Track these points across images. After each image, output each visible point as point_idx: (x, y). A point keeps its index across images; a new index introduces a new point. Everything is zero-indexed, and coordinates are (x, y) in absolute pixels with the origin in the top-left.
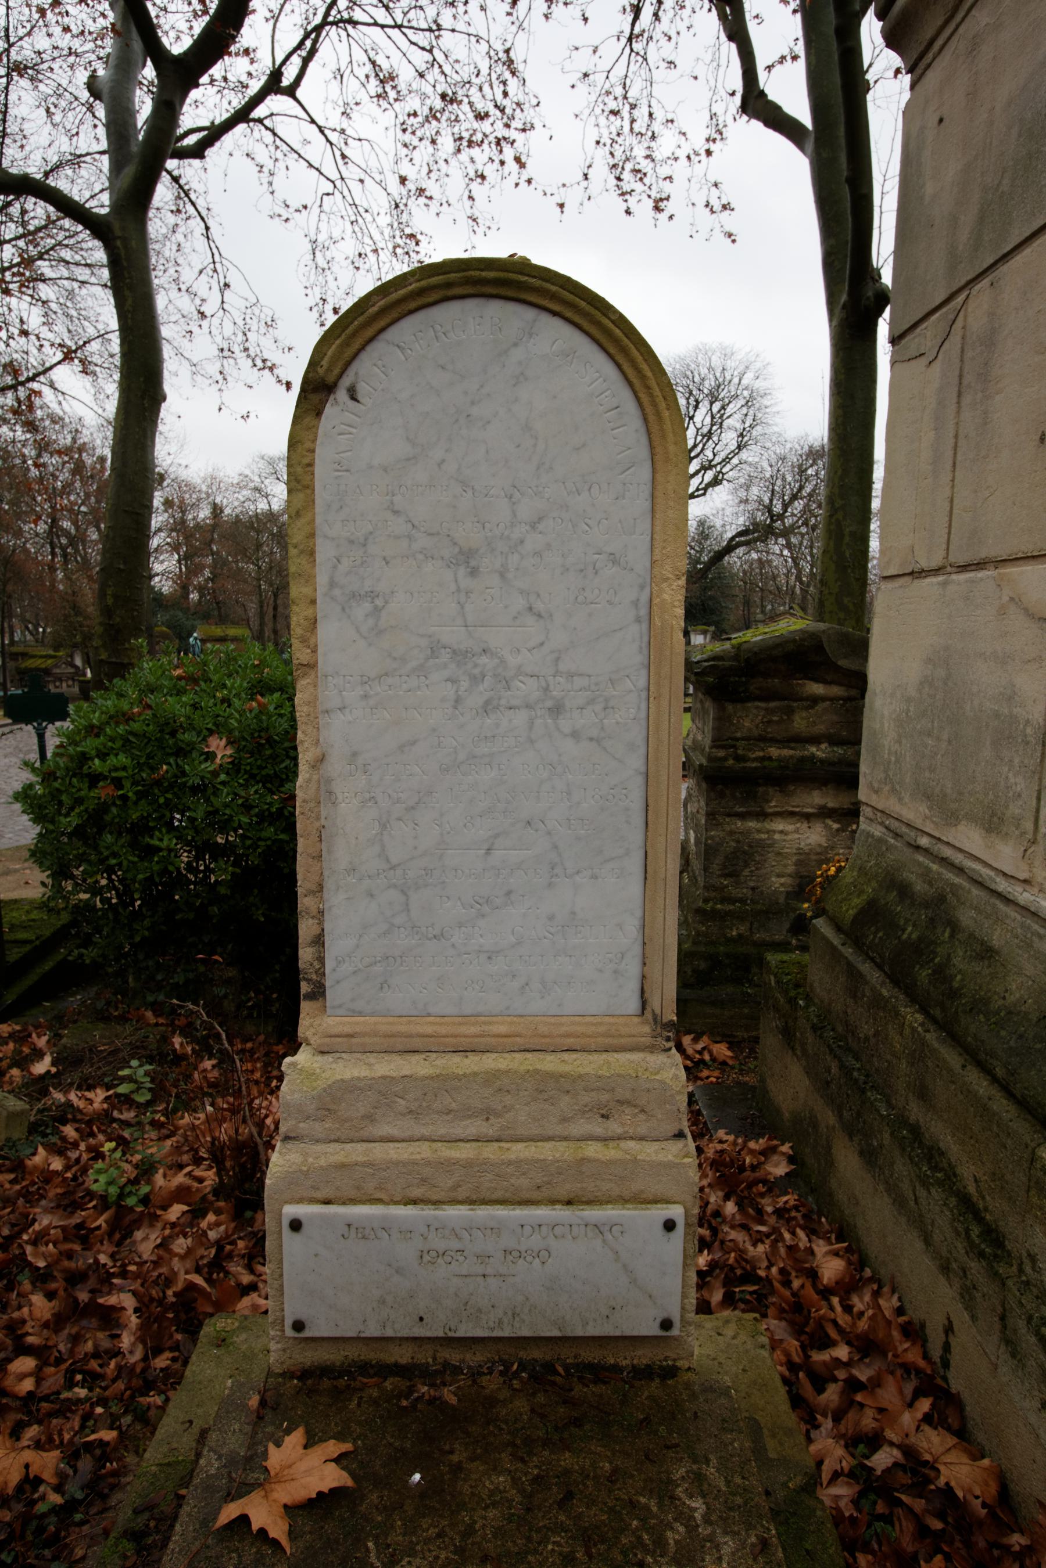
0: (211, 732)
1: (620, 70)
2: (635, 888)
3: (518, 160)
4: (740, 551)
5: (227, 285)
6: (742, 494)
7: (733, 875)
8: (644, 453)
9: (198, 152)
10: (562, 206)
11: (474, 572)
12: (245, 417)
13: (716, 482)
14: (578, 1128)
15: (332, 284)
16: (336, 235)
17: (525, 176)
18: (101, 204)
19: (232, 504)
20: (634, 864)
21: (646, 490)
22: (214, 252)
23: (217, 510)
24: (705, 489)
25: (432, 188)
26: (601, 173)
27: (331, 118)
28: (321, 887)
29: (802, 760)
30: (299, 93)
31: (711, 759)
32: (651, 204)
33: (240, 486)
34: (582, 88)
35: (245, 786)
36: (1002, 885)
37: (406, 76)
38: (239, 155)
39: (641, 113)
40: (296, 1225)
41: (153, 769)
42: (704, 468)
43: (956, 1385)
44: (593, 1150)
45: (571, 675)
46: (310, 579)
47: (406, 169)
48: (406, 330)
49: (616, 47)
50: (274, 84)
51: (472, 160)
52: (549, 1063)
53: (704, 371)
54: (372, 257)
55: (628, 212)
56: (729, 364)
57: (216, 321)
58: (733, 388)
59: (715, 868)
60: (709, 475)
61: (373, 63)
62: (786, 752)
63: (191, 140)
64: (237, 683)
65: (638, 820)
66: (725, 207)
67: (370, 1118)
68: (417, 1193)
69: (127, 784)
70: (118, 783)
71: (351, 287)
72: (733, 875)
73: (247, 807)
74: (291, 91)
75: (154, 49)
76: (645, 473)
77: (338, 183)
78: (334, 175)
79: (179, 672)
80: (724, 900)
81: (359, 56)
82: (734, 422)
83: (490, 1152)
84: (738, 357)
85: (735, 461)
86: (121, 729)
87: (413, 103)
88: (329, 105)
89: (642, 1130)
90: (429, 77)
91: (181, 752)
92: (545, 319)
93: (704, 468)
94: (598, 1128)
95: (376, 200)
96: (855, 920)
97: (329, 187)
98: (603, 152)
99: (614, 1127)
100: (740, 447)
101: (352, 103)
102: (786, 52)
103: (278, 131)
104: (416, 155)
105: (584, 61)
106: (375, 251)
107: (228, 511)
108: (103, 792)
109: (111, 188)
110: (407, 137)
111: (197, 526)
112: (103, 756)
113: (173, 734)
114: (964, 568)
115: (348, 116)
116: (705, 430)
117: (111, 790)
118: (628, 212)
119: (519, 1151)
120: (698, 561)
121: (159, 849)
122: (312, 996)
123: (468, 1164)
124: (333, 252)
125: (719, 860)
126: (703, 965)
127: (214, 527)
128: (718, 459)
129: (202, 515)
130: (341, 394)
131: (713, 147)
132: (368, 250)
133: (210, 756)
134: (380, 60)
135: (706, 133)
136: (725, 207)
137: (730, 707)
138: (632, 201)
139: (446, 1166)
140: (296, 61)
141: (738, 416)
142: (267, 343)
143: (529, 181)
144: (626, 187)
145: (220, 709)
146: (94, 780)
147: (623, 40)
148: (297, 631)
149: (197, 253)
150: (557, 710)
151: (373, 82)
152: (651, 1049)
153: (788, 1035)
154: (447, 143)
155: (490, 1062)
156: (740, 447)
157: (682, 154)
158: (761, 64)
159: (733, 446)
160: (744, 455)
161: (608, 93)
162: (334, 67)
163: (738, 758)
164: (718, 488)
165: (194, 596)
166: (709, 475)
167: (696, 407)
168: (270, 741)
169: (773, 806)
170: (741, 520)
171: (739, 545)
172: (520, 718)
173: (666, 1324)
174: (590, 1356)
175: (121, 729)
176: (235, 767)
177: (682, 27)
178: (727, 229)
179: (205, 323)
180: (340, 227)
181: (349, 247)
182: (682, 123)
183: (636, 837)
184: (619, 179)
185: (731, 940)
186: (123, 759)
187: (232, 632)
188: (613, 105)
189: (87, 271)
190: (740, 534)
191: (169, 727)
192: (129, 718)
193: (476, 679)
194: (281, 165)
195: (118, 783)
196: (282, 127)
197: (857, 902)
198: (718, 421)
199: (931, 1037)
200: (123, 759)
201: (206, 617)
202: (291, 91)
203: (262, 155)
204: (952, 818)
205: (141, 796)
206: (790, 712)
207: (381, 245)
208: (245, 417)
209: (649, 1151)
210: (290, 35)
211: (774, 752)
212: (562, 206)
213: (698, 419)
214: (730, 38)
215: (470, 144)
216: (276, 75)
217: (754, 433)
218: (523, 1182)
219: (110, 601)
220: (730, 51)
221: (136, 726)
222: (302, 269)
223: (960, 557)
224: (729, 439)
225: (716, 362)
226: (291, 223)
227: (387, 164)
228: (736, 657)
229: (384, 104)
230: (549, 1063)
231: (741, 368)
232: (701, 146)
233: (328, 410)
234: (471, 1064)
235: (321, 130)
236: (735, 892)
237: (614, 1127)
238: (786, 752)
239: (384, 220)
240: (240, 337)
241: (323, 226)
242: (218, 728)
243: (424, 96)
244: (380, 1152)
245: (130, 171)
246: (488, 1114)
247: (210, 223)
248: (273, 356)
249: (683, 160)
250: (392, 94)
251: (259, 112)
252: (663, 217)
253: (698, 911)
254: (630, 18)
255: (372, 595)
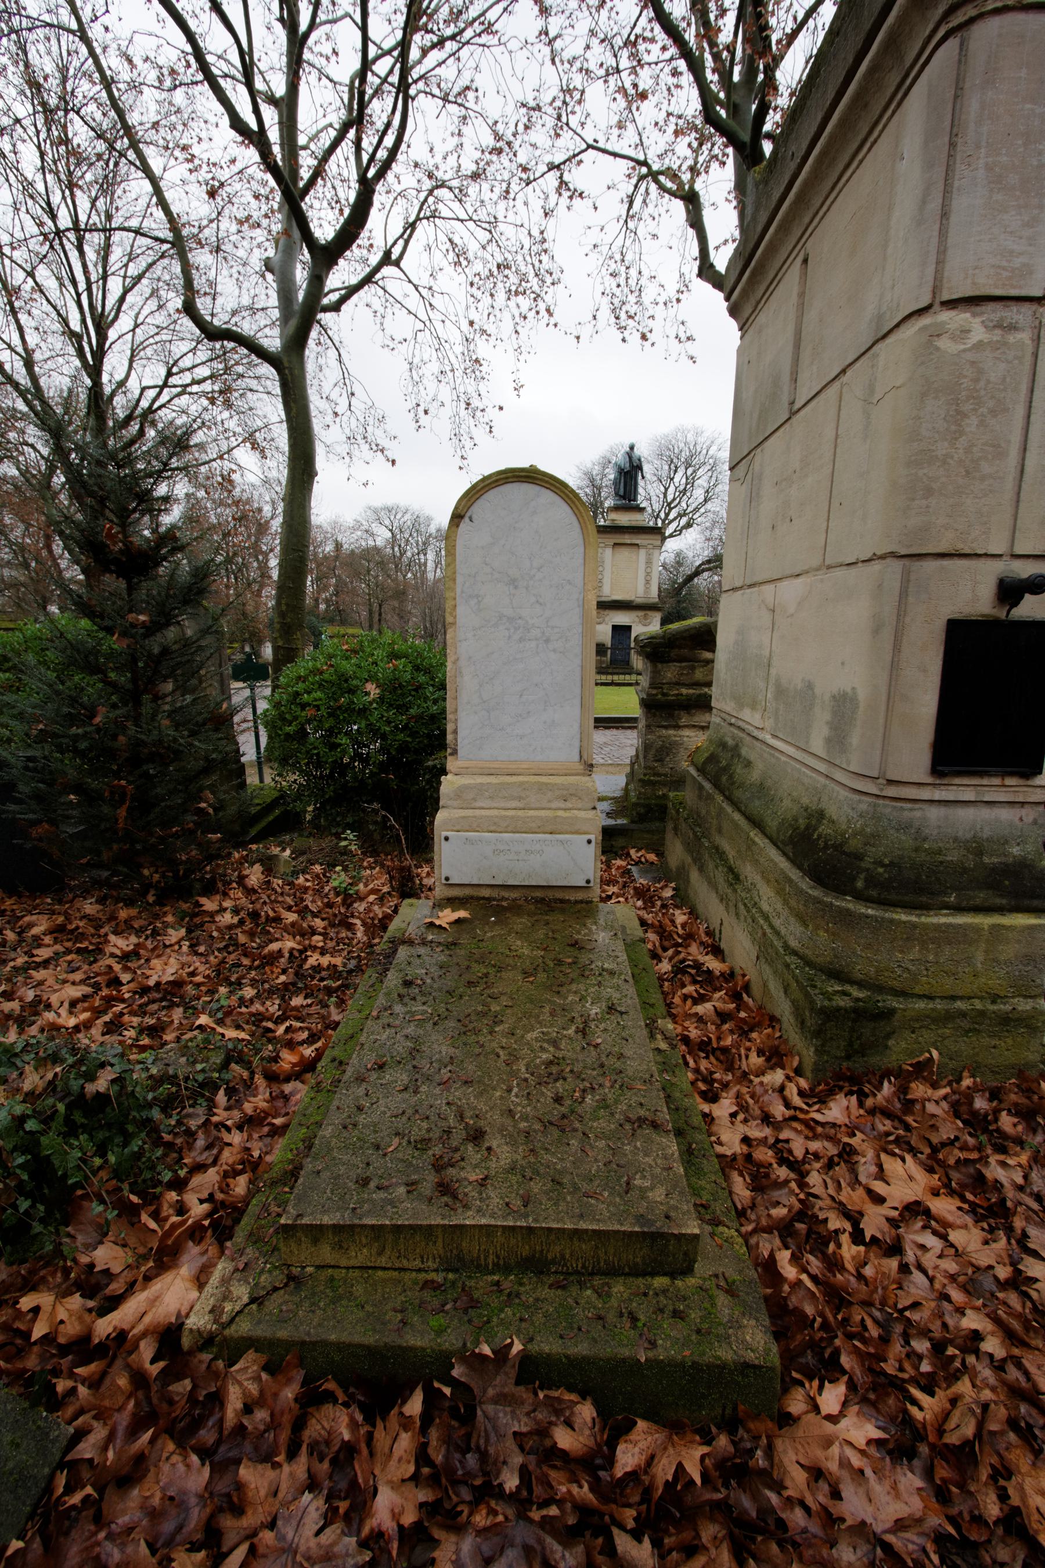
0: (367, 681)
1: (619, 242)
2: (577, 711)
3: (548, 311)
4: (706, 574)
5: (353, 394)
6: (708, 533)
7: (661, 760)
8: (581, 542)
9: (336, 307)
10: (578, 338)
11: (516, 587)
12: (365, 484)
13: (689, 525)
14: (554, 805)
15: (423, 392)
16: (426, 358)
17: (552, 321)
18: (272, 340)
19: (350, 541)
20: (577, 702)
21: (581, 556)
22: (345, 373)
23: (338, 546)
24: (681, 531)
25: (490, 328)
26: (605, 314)
27: (424, 280)
28: (456, 710)
29: (700, 695)
30: (402, 264)
31: (648, 695)
32: (639, 335)
33: (354, 529)
34: (593, 256)
35: (387, 711)
36: (756, 733)
37: (473, 247)
38: (361, 305)
39: (633, 272)
40: (447, 839)
41: (336, 700)
42: (680, 516)
43: (723, 945)
44: (560, 813)
45: (553, 628)
46: (453, 590)
47: (473, 315)
48: (492, 495)
49: (614, 228)
50: (387, 259)
51: (518, 306)
52: (544, 779)
53: (682, 445)
54: (450, 374)
55: (624, 340)
56: (700, 440)
57: (345, 418)
58: (702, 458)
59: (650, 756)
60: (684, 521)
61: (450, 240)
62: (691, 691)
63: (334, 297)
64: (379, 653)
65: (579, 684)
66: (688, 339)
67: (474, 799)
68: (492, 828)
69: (322, 708)
70: (318, 708)
71: (436, 396)
72: (661, 760)
73: (389, 722)
74: (397, 263)
75: (307, 236)
76: (582, 549)
77: (428, 323)
78: (425, 318)
79: (345, 647)
80: (655, 775)
81: (441, 238)
82: (702, 482)
83: (520, 813)
84: (705, 434)
85: (702, 510)
86: (317, 678)
87: (478, 267)
88: (422, 269)
89: (580, 806)
90: (489, 248)
91: (352, 691)
92: (544, 490)
93: (680, 516)
94: (562, 805)
95: (452, 335)
96: (704, 763)
97: (421, 326)
98: (606, 300)
99: (569, 805)
100: (706, 501)
101: (437, 268)
102: (728, 237)
103: (387, 289)
104: (480, 305)
105: (594, 236)
106: (452, 370)
107: (345, 546)
108: (309, 712)
109: (281, 337)
110: (474, 290)
111: (325, 557)
112: (309, 693)
113: (346, 681)
114: (750, 586)
115: (435, 278)
116: (682, 488)
117: (313, 712)
118: (624, 340)
119: (531, 813)
120: (675, 582)
121: (340, 745)
122: (451, 754)
123: (512, 817)
124: (424, 370)
125: (653, 752)
126: (642, 811)
127: (337, 557)
128: (690, 509)
129: (327, 549)
130: (466, 519)
131: (681, 296)
132: (448, 368)
133: (367, 694)
134: (457, 240)
135: (677, 287)
136: (688, 339)
137: (659, 666)
138: (626, 333)
139: (504, 818)
140: (401, 242)
141: (705, 478)
142: (379, 433)
143: (556, 325)
144: (623, 324)
145: (371, 668)
146: (303, 706)
147: (622, 222)
148: (448, 610)
149: (333, 373)
150: (547, 641)
151: (451, 254)
152: (583, 775)
153: (676, 829)
154: (501, 296)
155: (521, 778)
156: (706, 501)
157: (661, 300)
158: (711, 245)
159: (701, 499)
160: (709, 506)
161: (611, 258)
162: (425, 243)
163: (664, 695)
164: (690, 530)
165: (322, 607)
166: (684, 521)
167: (676, 471)
168: (401, 686)
169: (683, 721)
170: (706, 553)
171: (703, 571)
172: (533, 644)
173: (588, 882)
174: (559, 895)
175: (317, 678)
176: (381, 699)
177: (662, 211)
178: (690, 353)
179: (338, 420)
180: (428, 353)
181: (434, 367)
182: (661, 279)
183: (578, 691)
184: (617, 318)
185: (659, 797)
186: (319, 694)
187: (351, 631)
188: (613, 266)
189: (255, 382)
190: (703, 564)
191: (344, 678)
192: (321, 673)
193: (516, 629)
194: (389, 310)
195: (318, 708)
196: (390, 286)
197: (706, 755)
198: (691, 481)
199: (724, 805)
200: (319, 694)
201: (331, 621)
202: (397, 263)
203: (377, 304)
204: (741, 706)
205: (330, 715)
206: (693, 668)
207: (456, 366)
208: (365, 484)
209: (582, 814)
210: (396, 228)
211: (684, 691)
212: (578, 338)
213: (676, 480)
214: (692, 226)
215: (517, 293)
216: (388, 254)
217: (717, 490)
218: (534, 825)
219: (284, 608)
220: (691, 233)
221: (326, 676)
222: (403, 382)
223: (748, 582)
224: (699, 494)
225: (690, 438)
226: (395, 352)
227: (461, 313)
228: (663, 637)
229: (459, 270)
230: (544, 779)
231: (708, 443)
232: (674, 296)
233: (462, 525)
234: (514, 779)
235: (416, 287)
236: (661, 770)
237: (569, 805)
238: (691, 691)
239: (459, 349)
240: (362, 429)
241: (417, 352)
242: (371, 678)
243: (485, 262)
244: (478, 812)
245: (293, 323)
246: (520, 798)
247: (342, 351)
248: (384, 442)
249: (661, 305)
250: (464, 263)
251: (378, 276)
252: (648, 344)
253: (640, 780)
254: (626, 206)
255: (477, 596)
